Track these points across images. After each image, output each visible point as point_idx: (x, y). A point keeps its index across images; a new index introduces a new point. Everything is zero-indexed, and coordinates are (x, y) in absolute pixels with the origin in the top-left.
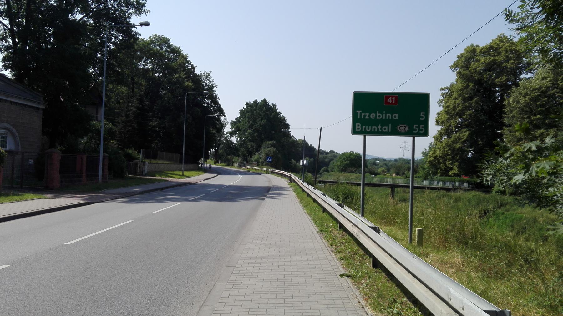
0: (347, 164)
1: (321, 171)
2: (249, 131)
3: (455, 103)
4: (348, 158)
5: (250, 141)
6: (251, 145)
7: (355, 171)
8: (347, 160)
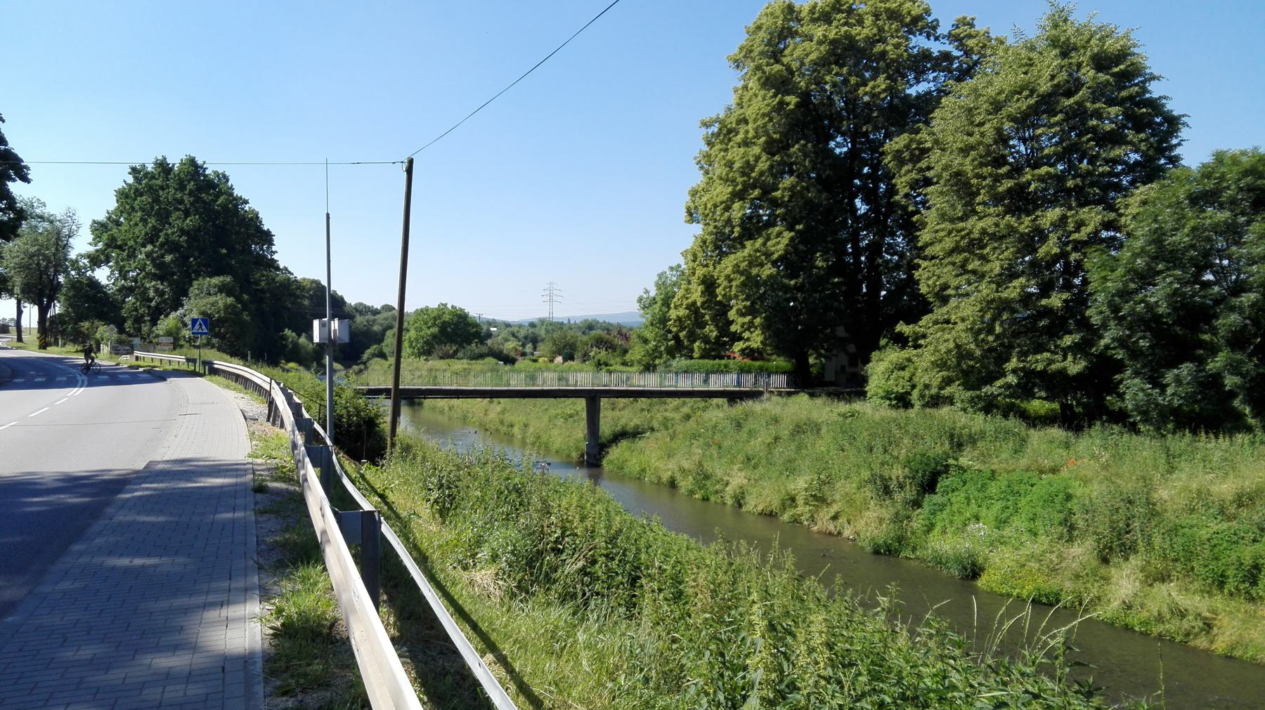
0: (434, 336)
1: (365, 356)
2: (149, 247)
3: (745, 154)
4: (435, 319)
5: (155, 277)
6: (156, 290)
7: (456, 352)
8: (434, 325)
